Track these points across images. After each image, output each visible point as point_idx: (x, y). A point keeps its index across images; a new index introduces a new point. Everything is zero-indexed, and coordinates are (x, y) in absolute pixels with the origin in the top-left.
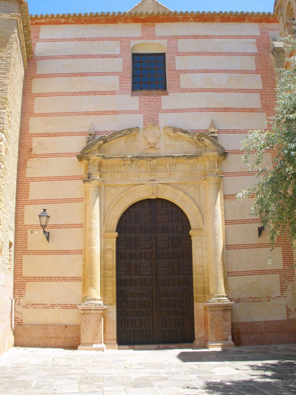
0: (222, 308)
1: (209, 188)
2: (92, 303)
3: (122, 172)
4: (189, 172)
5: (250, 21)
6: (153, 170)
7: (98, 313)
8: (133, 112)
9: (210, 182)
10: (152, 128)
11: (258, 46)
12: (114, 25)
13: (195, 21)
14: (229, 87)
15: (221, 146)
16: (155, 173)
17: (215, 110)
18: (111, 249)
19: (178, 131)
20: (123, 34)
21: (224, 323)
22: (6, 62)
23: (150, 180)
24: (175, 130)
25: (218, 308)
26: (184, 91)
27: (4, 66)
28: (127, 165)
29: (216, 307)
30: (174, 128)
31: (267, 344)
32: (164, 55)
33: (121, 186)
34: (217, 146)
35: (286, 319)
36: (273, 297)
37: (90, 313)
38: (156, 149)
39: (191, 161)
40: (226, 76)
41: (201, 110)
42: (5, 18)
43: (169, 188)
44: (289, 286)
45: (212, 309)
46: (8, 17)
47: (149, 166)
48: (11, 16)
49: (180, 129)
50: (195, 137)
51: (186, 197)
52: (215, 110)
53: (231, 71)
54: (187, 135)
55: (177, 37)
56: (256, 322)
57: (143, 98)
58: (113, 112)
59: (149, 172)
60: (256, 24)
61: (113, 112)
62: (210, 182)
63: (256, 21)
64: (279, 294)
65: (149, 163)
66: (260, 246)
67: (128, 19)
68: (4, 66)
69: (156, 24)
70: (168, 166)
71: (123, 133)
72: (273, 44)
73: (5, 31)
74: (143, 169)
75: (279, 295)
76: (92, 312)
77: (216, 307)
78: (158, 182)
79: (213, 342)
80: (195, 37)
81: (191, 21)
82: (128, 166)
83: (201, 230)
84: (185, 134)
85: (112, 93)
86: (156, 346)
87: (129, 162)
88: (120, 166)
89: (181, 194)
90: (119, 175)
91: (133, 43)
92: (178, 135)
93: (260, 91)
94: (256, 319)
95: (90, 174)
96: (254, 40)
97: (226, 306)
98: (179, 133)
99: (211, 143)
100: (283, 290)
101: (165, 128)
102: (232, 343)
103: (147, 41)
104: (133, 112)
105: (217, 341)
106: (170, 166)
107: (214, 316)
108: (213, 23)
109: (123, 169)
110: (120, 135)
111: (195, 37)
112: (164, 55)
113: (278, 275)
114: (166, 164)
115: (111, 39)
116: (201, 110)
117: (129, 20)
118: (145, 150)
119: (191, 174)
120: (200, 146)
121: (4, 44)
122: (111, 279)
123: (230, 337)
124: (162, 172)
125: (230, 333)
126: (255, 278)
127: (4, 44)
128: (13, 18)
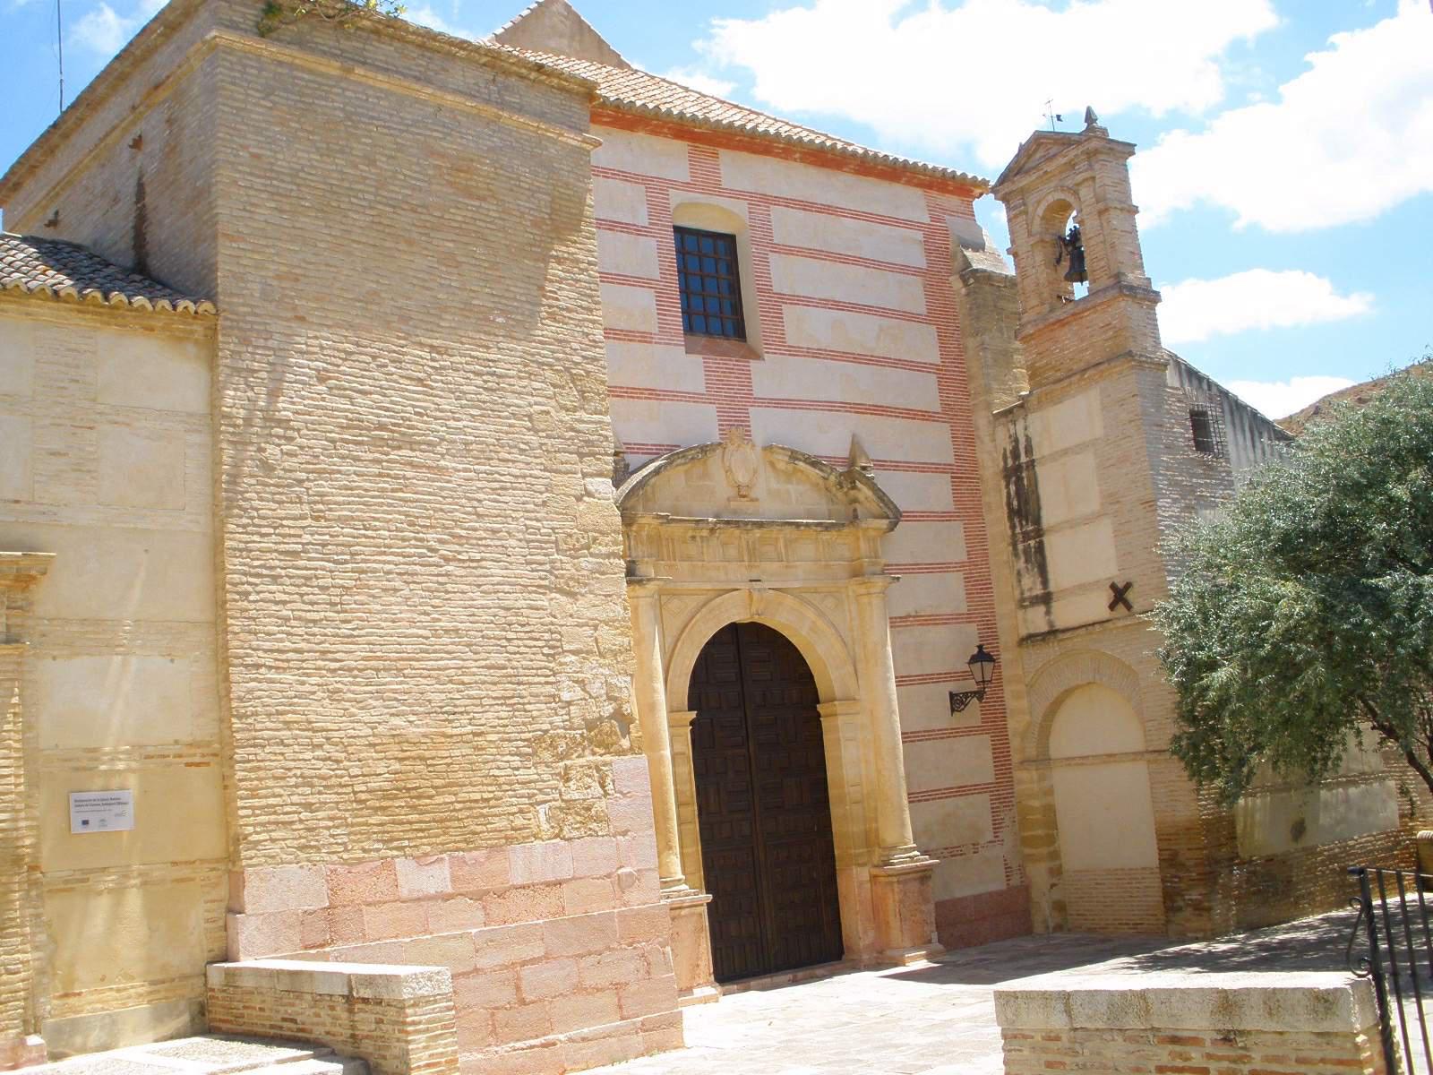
0: (920, 874)
1: (870, 603)
2: (680, 891)
3: (689, 558)
4: (823, 563)
5: (909, 183)
6: (753, 554)
7: (694, 914)
8: (694, 397)
9: (872, 590)
10: (739, 446)
11: (928, 252)
12: (626, 134)
13: (802, 160)
14: (879, 353)
15: (896, 507)
16: (756, 564)
17: (859, 409)
18: (684, 754)
19: (797, 459)
20: (648, 168)
21: (923, 908)
22: (589, 275)
23: (751, 581)
24: (794, 456)
25: (914, 875)
26: (794, 351)
27: (585, 288)
28: (698, 539)
29: (909, 873)
30: (792, 451)
31: (981, 944)
32: (730, 239)
33: (691, 593)
34: (886, 505)
35: (1004, 887)
36: (982, 842)
37: (679, 915)
38: (752, 500)
39: (826, 536)
40: (874, 322)
41: (831, 406)
42: (567, 144)
43: (789, 600)
44: (1007, 818)
45: (902, 878)
46: (575, 143)
47: (744, 543)
48: (583, 142)
49: (804, 455)
50: (832, 478)
51: (820, 623)
52: (859, 409)
53: (883, 312)
54: (817, 471)
55: (768, 200)
56: (959, 899)
57: (716, 362)
58: (653, 394)
59: (746, 558)
60: (919, 191)
61: (653, 394)
62: (872, 590)
63: (921, 185)
64: (989, 836)
65: (744, 536)
66: (955, 733)
67: (663, 127)
68: (585, 288)
69: (722, 152)
70: (781, 544)
71: (690, 454)
72: (965, 256)
73: (572, 180)
74: (732, 552)
75: (992, 838)
76: (683, 912)
77: (909, 873)
78: (767, 585)
79: (910, 950)
80: (806, 206)
81: (795, 160)
82: (702, 542)
83: (854, 699)
84: (813, 469)
85: (645, 338)
86: (790, 976)
87: (705, 533)
88: (684, 542)
89: (810, 614)
90: (686, 564)
91: (676, 197)
92: (796, 470)
93: (935, 369)
94: (958, 895)
95: (634, 562)
96: (920, 236)
97: (925, 870)
98: (801, 464)
99: (874, 498)
100: (997, 827)
101: (768, 448)
102: (941, 947)
103: (702, 198)
104: (694, 397)
105: (915, 947)
106: (786, 546)
107: (905, 893)
108: (838, 173)
109: (692, 549)
110: (683, 461)
111: (806, 206)
112: (730, 239)
113: (986, 796)
114: (777, 539)
115: (626, 176)
116: (831, 406)
117: (666, 130)
118: (729, 500)
119: (827, 566)
120: (834, 499)
121: (575, 222)
122: (691, 826)
123: (935, 936)
124: (771, 560)
125: (934, 928)
126: (949, 804)
127: (575, 222)
128: (584, 145)
